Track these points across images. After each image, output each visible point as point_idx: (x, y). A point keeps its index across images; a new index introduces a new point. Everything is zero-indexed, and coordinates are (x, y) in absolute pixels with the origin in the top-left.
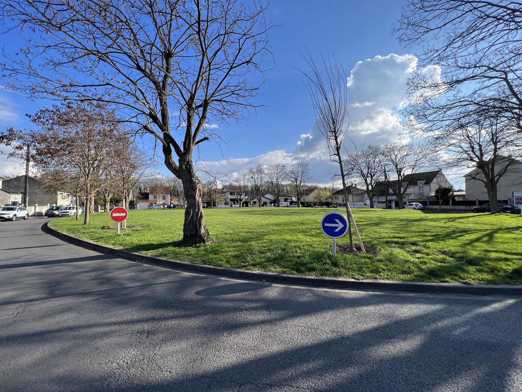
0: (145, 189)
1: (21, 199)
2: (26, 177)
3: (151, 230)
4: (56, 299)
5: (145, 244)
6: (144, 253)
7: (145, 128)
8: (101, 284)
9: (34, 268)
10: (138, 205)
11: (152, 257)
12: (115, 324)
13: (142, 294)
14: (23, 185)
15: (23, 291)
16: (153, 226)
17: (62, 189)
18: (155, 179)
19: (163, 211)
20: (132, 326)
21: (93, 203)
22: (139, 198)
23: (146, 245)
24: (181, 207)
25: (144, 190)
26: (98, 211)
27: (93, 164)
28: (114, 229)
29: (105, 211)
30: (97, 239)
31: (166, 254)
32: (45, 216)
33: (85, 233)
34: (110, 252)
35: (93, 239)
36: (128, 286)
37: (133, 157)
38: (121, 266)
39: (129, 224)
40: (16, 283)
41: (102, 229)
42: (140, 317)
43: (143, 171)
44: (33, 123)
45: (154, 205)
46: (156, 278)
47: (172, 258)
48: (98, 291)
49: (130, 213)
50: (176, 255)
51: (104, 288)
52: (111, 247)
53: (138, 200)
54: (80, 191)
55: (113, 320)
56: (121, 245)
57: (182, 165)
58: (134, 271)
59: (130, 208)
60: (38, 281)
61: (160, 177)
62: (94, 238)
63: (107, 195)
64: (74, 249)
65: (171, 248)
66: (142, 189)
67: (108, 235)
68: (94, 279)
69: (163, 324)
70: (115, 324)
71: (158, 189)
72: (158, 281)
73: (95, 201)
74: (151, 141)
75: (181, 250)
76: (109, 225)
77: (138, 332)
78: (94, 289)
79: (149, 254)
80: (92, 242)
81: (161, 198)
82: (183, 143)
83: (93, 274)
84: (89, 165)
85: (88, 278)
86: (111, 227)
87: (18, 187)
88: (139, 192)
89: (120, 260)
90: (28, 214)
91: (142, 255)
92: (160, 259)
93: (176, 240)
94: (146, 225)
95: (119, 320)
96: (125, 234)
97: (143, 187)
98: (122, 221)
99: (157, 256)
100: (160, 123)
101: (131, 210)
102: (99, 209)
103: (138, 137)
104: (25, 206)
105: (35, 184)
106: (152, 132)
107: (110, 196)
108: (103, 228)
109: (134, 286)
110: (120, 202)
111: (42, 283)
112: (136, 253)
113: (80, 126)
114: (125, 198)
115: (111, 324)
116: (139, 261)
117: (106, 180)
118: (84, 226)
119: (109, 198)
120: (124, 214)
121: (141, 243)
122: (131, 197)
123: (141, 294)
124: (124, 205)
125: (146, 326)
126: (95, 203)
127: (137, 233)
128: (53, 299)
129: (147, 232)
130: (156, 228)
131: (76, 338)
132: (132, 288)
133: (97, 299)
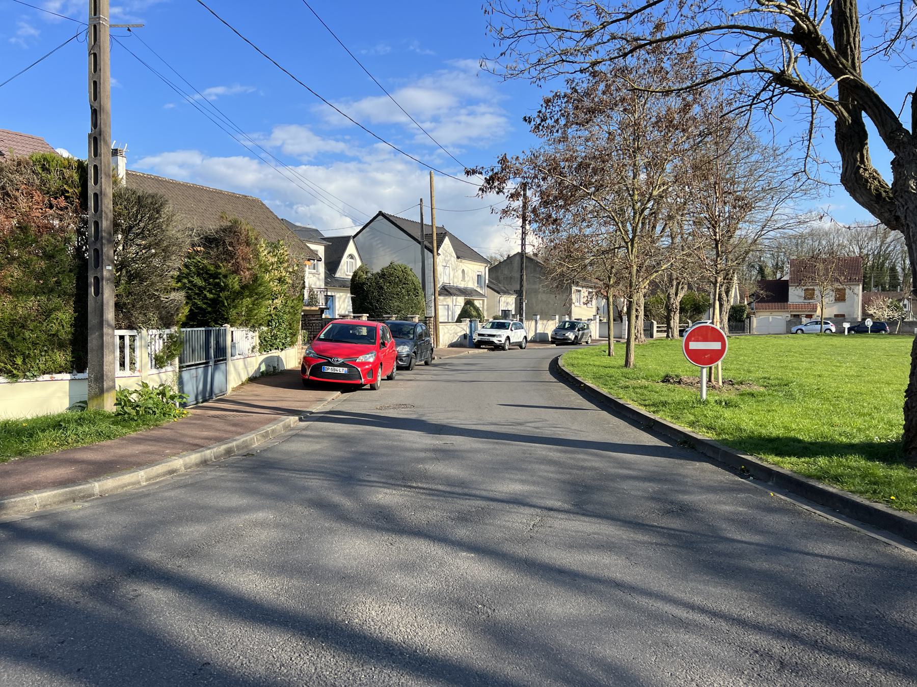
0: (777, 267)
1: (514, 305)
2: (522, 255)
3: (790, 396)
4: (587, 519)
5: (774, 435)
6: (770, 461)
7: (781, 79)
8: (668, 512)
9: (547, 448)
10: (755, 321)
11: (796, 476)
12: (703, 610)
13: (766, 566)
14: (517, 275)
15: (537, 489)
16: (801, 386)
17: (584, 281)
18: (811, 234)
19: (837, 341)
20: (741, 632)
21: (642, 313)
22: (758, 297)
23: (777, 439)
24: (908, 328)
25: (775, 274)
26: (652, 336)
27: (643, 211)
28: (692, 384)
29: (668, 336)
30: (654, 405)
31: (842, 475)
32: (552, 342)
33: (627, 387)
34: (685, 442)
35: (645, 406)
36: (729, 535)
37: (741, 172)
38: (711, 483)
39: (731, 375)
40: (525, 470)
41: (663, 382)
42: (760, 619)
43: (770, 213)
44: (533, 135)
45: (804, 320)
46: (804, 536)
47: (861, 493)
48: (662, 528)
49: (733, 342)
50: (875, 485)
51: (675, 523)
52: (687, 430)
53: (754, 305)
54: (617, 283)
55: (697, 600)
56: (710, 428)
57: (907, 179)
58: (743, 504)
59: (732, 329)
60: (556, 476)
61: (826, 224)
62: (647, 403)
63: (672, 291)
64: (609, 423)
65: (857, 462)
66: (768, 271)
67: (677, 399)
68: (652, 499)
69: (823, 660)
70: (703, 610)
71: (820, 266)
72: (812, 546)
73: (645, 307)
74: (798, 117)
75: (891, 472)
76: (679, 372)
77: (756, 652)
78: (654, 521)
79: (787, 465)
80: (643, 411)
81: (829, 298)
82: (910, 98)
83: (651, 487)
84: (635, 213)
85: (640, 493)
86: (684, 378)
87: (510, 279)
88: (759, 278)
89: (707, 466)
90: (525, 337)
91: (765, 464)
92: (821, 486)
93: (876, 439)
94: (777, 382)
95: (710, 604)
96: (721, 402)
97: (770, 263)
98: (713, 365)
99: (810, 476)
100: (828, 51)
101: (734, 336)
102: (655, 329)
103: (757, 113)
104: (521, 320)
105: (535, 270)
106: (801, 88)
107: (681, 295)
108: (666, 379)
109: (744, 539)
110: (705, 311)
111: (564, 482)
112: (749, 458)
113: (617, 115)
114: (720, 299)
115: (691, 607)
116: (757, 479)
117: (671, 248)
118: (625, 370)
119: (679, 299)
120: (716, 346)
121: (764, 432)
122: (736, 296)
123: (762, 564)
124: (718, 320)
125: (777, 647)
126: (645, 315)
127: (751, 401)
128: (582, 518)
129: (781, 404)
130: (809, 394)
131: (628, 606)
132: (739, 546)
133: (661, 545)
